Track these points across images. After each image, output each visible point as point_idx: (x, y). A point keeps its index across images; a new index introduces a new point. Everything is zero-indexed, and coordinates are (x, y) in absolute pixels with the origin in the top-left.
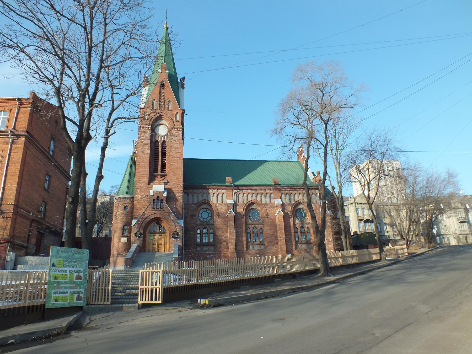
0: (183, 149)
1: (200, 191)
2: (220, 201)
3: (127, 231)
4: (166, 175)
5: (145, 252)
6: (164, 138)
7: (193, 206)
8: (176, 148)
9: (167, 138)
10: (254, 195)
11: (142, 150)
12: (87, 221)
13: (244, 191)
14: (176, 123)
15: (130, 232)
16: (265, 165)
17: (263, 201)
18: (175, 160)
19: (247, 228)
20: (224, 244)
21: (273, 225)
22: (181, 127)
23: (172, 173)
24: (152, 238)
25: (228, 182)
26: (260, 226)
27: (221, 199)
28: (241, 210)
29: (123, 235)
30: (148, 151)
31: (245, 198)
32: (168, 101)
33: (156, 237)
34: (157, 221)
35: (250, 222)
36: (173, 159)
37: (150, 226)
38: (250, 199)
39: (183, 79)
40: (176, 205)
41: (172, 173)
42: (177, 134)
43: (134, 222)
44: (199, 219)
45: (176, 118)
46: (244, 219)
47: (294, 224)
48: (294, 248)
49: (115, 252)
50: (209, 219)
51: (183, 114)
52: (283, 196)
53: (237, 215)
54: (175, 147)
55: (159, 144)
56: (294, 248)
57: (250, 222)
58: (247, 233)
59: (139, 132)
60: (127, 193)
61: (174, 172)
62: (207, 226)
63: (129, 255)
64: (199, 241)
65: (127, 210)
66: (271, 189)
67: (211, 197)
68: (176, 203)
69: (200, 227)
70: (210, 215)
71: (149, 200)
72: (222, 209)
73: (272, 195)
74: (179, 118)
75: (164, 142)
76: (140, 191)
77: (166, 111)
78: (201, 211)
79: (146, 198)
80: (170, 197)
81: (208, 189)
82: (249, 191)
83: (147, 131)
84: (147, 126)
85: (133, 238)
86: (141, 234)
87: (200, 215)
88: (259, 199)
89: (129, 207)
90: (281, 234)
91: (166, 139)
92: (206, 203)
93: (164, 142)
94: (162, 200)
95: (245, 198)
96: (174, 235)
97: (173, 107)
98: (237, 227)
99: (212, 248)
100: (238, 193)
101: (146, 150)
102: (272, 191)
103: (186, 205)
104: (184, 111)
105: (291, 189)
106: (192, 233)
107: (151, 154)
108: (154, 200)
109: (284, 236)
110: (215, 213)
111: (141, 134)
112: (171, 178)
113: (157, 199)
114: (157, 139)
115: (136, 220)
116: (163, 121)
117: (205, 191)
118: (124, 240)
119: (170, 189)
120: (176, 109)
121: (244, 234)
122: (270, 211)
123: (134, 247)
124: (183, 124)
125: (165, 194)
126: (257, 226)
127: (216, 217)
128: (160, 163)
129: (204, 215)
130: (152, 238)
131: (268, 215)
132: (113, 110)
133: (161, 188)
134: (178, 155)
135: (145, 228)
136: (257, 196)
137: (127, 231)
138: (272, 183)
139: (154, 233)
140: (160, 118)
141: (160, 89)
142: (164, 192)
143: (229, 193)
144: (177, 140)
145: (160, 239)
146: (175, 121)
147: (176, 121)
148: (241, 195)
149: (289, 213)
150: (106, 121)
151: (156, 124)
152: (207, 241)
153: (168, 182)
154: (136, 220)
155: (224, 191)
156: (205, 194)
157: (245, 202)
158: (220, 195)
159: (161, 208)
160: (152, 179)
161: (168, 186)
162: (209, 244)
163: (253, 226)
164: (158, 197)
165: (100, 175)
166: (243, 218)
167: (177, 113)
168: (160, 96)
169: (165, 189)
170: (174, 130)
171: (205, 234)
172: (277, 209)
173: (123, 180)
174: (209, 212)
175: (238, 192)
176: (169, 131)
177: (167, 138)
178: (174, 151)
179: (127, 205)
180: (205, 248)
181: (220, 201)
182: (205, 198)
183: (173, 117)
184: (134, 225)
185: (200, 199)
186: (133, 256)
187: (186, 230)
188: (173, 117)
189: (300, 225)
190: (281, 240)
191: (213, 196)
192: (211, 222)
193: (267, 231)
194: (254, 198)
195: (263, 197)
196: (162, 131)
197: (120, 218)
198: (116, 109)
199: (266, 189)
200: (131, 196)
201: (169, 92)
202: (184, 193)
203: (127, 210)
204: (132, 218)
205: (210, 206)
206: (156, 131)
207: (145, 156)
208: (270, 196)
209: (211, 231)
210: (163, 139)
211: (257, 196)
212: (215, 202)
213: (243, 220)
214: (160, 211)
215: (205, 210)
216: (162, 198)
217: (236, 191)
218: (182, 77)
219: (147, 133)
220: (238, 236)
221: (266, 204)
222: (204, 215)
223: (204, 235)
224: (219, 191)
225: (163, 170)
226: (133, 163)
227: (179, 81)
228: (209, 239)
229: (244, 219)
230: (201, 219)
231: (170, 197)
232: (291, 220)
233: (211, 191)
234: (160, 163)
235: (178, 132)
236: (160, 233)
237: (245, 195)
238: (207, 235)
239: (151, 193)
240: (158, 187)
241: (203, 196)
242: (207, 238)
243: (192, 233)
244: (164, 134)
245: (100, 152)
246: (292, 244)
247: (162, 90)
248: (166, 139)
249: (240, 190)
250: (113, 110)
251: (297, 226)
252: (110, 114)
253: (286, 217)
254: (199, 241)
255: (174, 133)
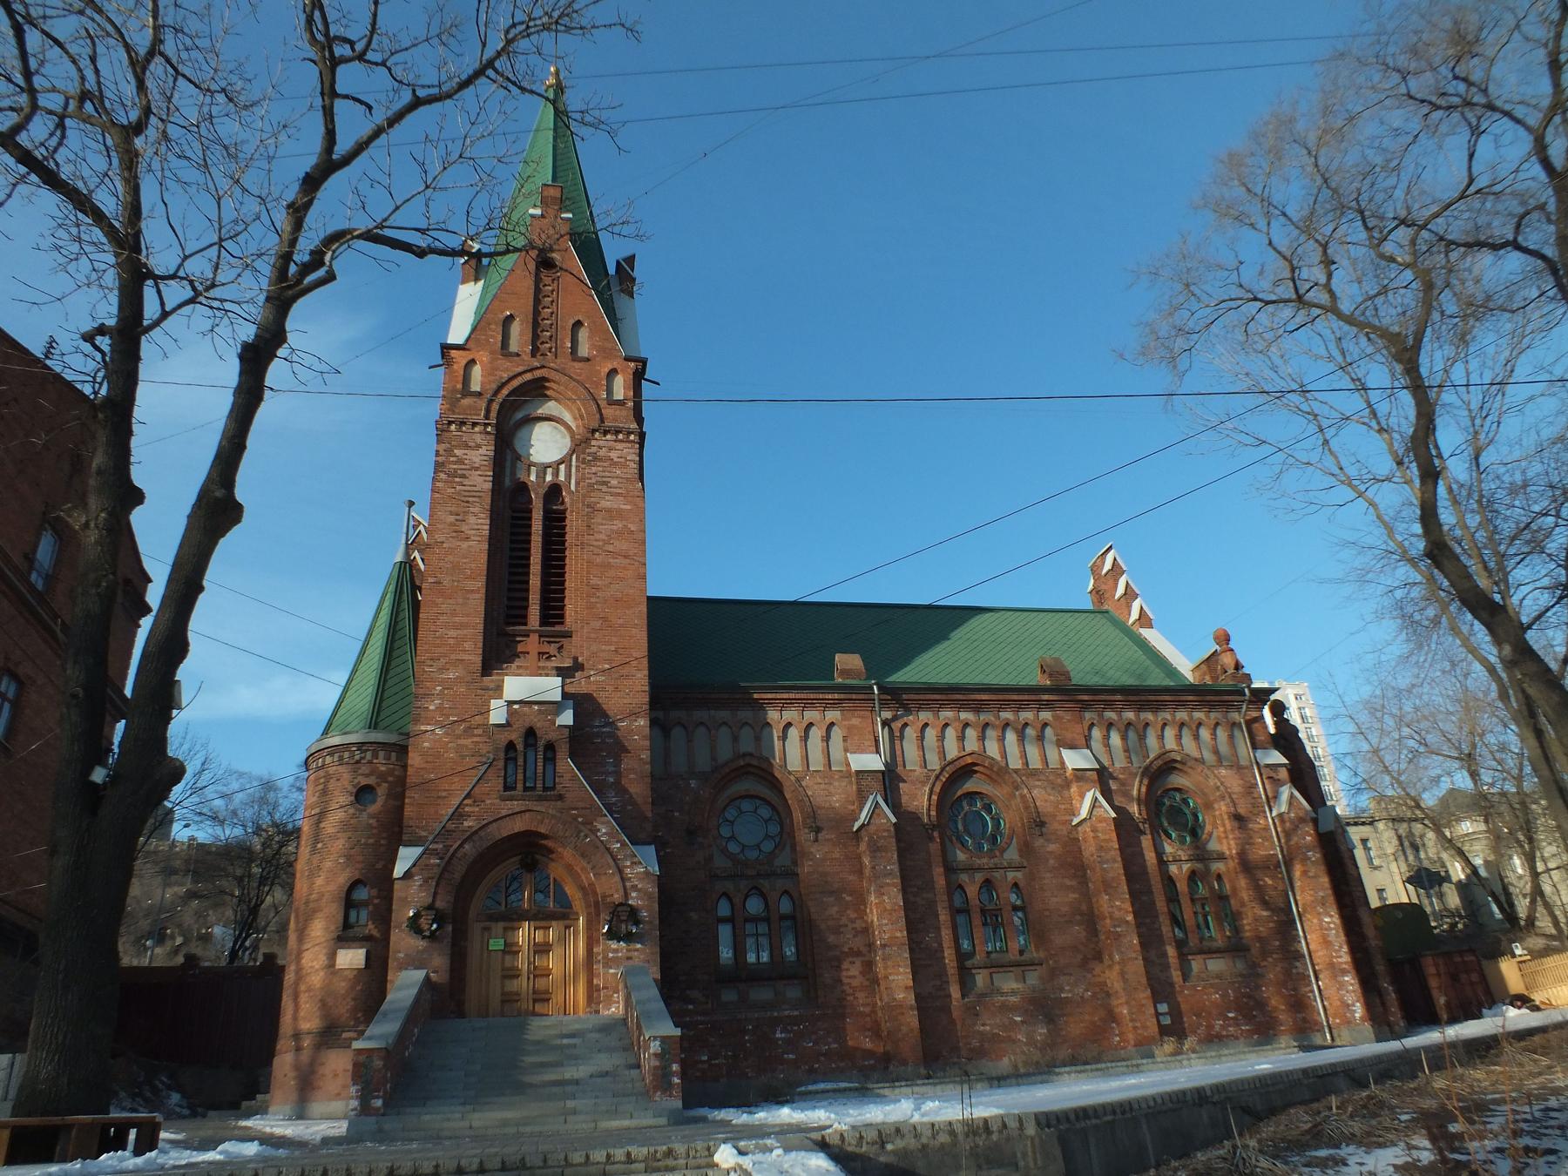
0: (642, 521)
1: (724, 714)
2: (817, 762)
3: (364, 914)
4: (568, 635)
5: (461, 1013)
6: (556, 474)
7: (693, 783)
8: (612, 514)
9: (568, 476)
10: (971, 733)
11: (452, 519)
12: (99, 775)
13: (924, 716)
14: (608, 412)
15: (384, 917)
16: (976, 622)
17: (1015, 763)
18: (609, 566)
19: (955, 888)
20: (852, 972)
21: (1075, 865)
22: (634, 426)
23: (597, 624)
24: (497, 944)
25: (846, 673)
26: (1011, 875)
27: (824, 751)
28: (920, 799)
29: (345, 936)
30: (478, 523)
31: (933, 744)
32: (572, 321)
33: (524, 934)
34: (528, 851)
35: (961, 856)
36: (598, 560)
37: (495, 878)
38: (952, 751)
39: (631, 260)
40: (618, 774)
41: (597, 624)
42: (613, 455)
43: (406, 858)
44: (724, 851)
45: (610, 391)
46: (943, 835)
47: (1162, 863)
48: (1176, 975)
49: (309, 1021)
50: (768, 847)
51: (639, 376)
52: (1096, 733)
53: (907, 823)
54: (609, 511)
55: (530, 501)
56: (1176, 975)
57: (961, 856)
58: (955, 912)
59: (439, 442)
60: (374, 724)
61: (605, 619)
62: (765, 884)
63: (383, 1031)
64: (726, 954)
65: (374, 808)
66: (1048, 705)
67: (777, 744)
68: (617, 763)
69: (729, 886)
70: (774, 829)
71: (484, 749)
72: (836, 797)
73: (1048, 731)
74: (620, 388)
75: (555, 491)
76: (440, 708)
77: (564, 361)
78: (731, 813)
79: (467, 742)
80: (591, 732)
81: (759, 707)
82: (947, 714)
83: (478, 439)
84: (475, 418)
85: (403, 942)
86: (439, 918)
87: (725, 831)
88: (993, 749)
89: (382, 791)
90: (1117, 907)
91: (562, 477)
92: (759, 771)
93: (555, 491)
94: (550, 747)
95: (933, 744)
96: (622, 923)
97: (593, 347)
98: (912, 882)
99: (793, 992)
100: (897, 725)
101: (472, 520)
102: (1046, 715)
103: (662, 778)
104: (644, 362)
105: (1130, 705)
106: (694, 916)
107: (492, 540)
108: (511, 746)
109: (1130, 918)
110: (797, 816)
111: (449, 452)
112: (594, 648)
113: (526, 745)
114: (521, 476)
115: (418, 851)
116: (552, 404)
117: (745, 714)
118: (352, 958)
119: (588, 698)
120: (608, 353)
121: (944, 916)
122: (1042, 797)
123: (405, 985)
124: (639, 420)
125: (567, 718)
126: (997, 875)
127: (804, 836)
128: (535, 581)
129: (746, 831)
130: (497, 944)
131: (1042, 824)
132: (328, 166)
133: (549, 687)
134: (621, 545)
135: (464, 892)
136: (982, 738)
137: (364, 914)
138: (1036, 678)
139: (513, 917)
140: (536, 389)
141: (538, 281)
142: (557, 707)
143: (855, 721)
144: (614, 482)
145: (543, 949)
146: (603, 404)
147: (612, 402)
148: (910, 733)
149: (1134, 809)
150: (281, 218)
151: (519, 415)
152: (765, 957)
153: (578, 666)
154: (418, 851)
155: (833, 715)
156: (746, 730)
157: (934, 763)
158: (816, 734)
159: (545, 789)
160: (498, 652)
161: (580, 685)
162: (776, 973)
163: (979, 877)
164: (530, 733)
165: (219, 493)
166: (931, 839)
167: (613, 372)
168: (537, 301)
169: (565, 695)
170: (599, 441)
171: (755, 920)
172: (1082, 796)
173: (354, 671)
174: (765, 812)
175: (895, 718)
176: (579, 445)
177: (568, 476)
178: (604, 528)
179: (371, 781)
180: (762, 994)
181: (817, 762)
182: (746, 745)
183: (597, 384)
184: (408, 875)
185: (725, 752)
186: (402, 1036)
187: (668, 895)
188: (597, 384)
189: (1186, 867)
190: (1118, 936)
191: (784, 738)
192: (782, 860)
193: (1056, 897)
194: (972, 744)
195: (1011, 737)
196: (546, 445)
197: (340, 844)
198: (347, 160)
199: (1020, 706)
200: (392, 738)
201: (574, 296)
202: (654, 722)
203: (374, 808)
204: (394, 832)
205: (776, 785)
206: (518, 446)
207: (465, 545)
208: (1040, 738)
209: (785, 906)
210: (549, 478)
211: (982, 738)
212: (794, 762)
213: (934, 847)
214: (540, 799)
215: (746, 805)
216: (553, 736)
217: (887, 715)
218: (628, 254)
219: (478, 446)
220: (917, 921)
221: (1028, 773)
222: (746, 831)
223: (750, 928)
224: (811, 715)
225: (553, 611)
226: (407, 589)
227: (612, 270)
228: (775, 950)
229: (943, 835)
230: (733, 848)
231: (591, 732)
232: (1146, 842)
233: (773, 715)
234: (535, 581)
235: (619, 446)
236: (541, 917)
237: (931, 734)
238: (763, 928)
239: (498, 715)
240: (524, 685)
241: (735, 739)
242: (764, 941)
243: (694, 916)
244: (556, 457)
245: (230, 371)
246: (1165, 955)
247: (547, 280)
248: (562, 477)
249: (908, 711)
250: (328, 166)
251: (1173, 869)
252: (312, 183)
253: (1123, 823)
254: (726, 954)
255: (602, 453)
